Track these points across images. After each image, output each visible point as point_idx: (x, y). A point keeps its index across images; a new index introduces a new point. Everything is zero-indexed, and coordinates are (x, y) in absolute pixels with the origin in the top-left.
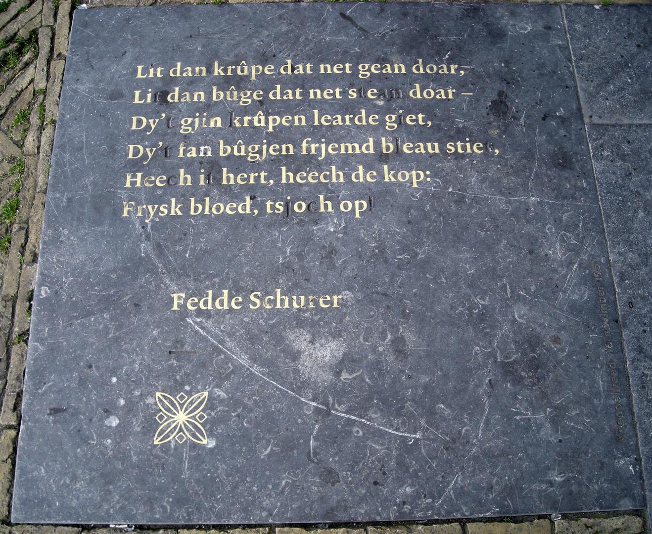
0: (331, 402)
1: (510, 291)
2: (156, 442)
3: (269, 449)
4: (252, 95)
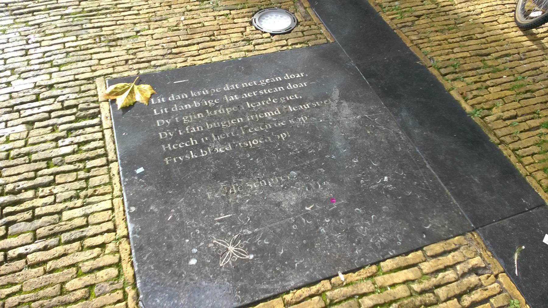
0: (304, 221)
1: (137, 264)
2: (221, 265)
3: (282, 251)
4: (214, 101)
